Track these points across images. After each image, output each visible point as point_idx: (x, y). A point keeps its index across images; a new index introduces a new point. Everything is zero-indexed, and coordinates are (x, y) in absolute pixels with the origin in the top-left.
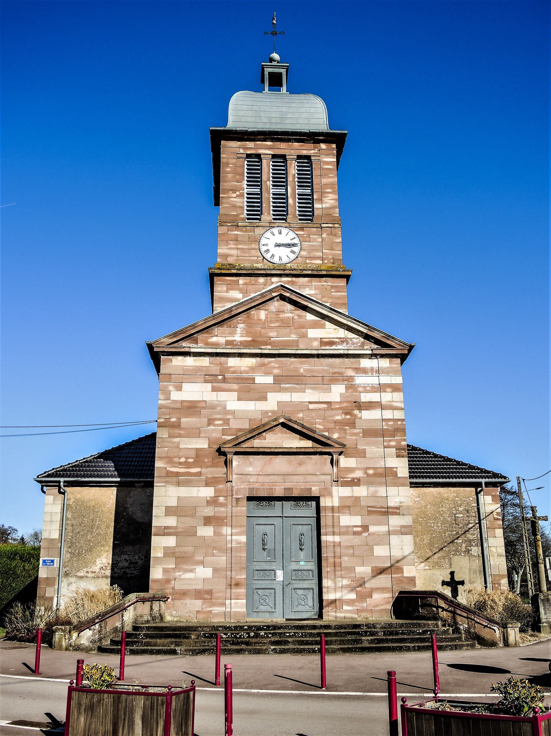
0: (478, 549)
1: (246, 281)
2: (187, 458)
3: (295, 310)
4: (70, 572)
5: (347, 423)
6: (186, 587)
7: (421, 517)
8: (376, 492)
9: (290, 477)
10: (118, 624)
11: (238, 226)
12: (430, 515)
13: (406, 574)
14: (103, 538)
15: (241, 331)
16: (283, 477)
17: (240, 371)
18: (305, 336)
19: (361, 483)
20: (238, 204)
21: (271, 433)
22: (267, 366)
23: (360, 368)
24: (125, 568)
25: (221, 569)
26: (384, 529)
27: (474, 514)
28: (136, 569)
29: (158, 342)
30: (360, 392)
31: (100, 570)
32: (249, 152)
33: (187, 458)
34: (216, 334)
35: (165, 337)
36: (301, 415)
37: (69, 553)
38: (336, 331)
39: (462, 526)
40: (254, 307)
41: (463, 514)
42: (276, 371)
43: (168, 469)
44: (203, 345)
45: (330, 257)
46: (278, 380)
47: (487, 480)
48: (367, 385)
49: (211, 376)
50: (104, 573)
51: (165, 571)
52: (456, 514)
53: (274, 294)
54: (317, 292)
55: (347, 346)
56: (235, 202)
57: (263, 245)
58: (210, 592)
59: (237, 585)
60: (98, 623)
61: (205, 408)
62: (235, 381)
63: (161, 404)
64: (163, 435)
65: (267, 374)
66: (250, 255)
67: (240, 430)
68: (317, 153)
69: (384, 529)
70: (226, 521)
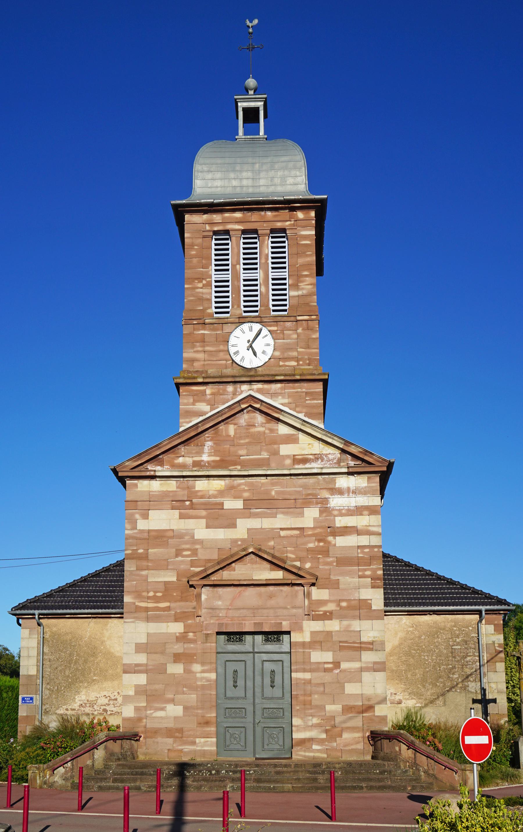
0: (476, 685)
1: (213, 391)
2: (155, 592)
3: (268, 422)
4: (50, 710)
5: (320, 551)
6: (157, 725)
7: (414, 650)
8: (349, 626)
9: (260, 611)
10: (89, 762)
11: (204, 324)
12: (424, 647)
13: (377, 714)
14: (81, 674)
15: (209, 450)
16: (253, 611)
17: (208, 496)
18: (276, 453)
19: (333, 616)
20: (205, 296)
21: (241, 563)
22: (237, 488)
23: (335, 489)
24: (105, 705)
25: (192, 707)
26: (356, 665)
27: (473, 646)
28: (116, 705)
29: (122, 466)
30: (335, 516)
31: (80, 707)
32: (216, 229)
33: (155, 592)
34: (183, 453)
35: (128, 460)
36: (272, 543)
37: (48, 690)
38: (310, 446)
39: (459, 659)
40: (223, 421)
41: (461, 646)
42: (246, 495)
43: (137, 604)
44: (169, 467)
45: (306, 357)
46: (248, 504)
47: (488, 607)
48: (342, 508)
49: (178, 502)
50: (84, 711)
51: (137, 709)
52: (453, 646)
53: (243, 406)
54: (290, 400)
55: (322, 463)
56: (203, 293)
57: (233, 346)
58: (181, 730)
59: (207, 723)
60: (70, 761)
61: (173, 537)
62: (203, 507)
63: (128, 535)
64: (130, 568)
65: (236, 497)
66: (218, 358)
67: (209, 561)
68: (294, 225)
69: (356, 665)
70: (195, 657)
